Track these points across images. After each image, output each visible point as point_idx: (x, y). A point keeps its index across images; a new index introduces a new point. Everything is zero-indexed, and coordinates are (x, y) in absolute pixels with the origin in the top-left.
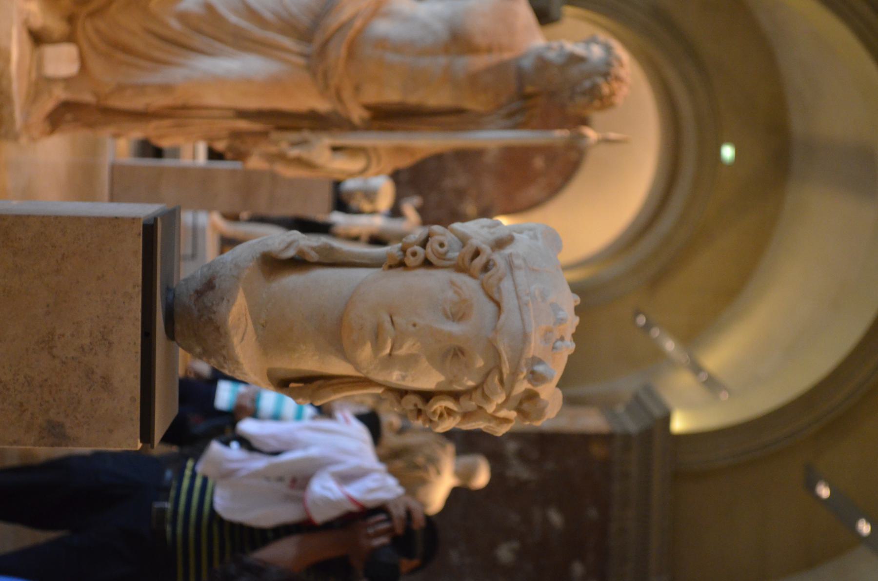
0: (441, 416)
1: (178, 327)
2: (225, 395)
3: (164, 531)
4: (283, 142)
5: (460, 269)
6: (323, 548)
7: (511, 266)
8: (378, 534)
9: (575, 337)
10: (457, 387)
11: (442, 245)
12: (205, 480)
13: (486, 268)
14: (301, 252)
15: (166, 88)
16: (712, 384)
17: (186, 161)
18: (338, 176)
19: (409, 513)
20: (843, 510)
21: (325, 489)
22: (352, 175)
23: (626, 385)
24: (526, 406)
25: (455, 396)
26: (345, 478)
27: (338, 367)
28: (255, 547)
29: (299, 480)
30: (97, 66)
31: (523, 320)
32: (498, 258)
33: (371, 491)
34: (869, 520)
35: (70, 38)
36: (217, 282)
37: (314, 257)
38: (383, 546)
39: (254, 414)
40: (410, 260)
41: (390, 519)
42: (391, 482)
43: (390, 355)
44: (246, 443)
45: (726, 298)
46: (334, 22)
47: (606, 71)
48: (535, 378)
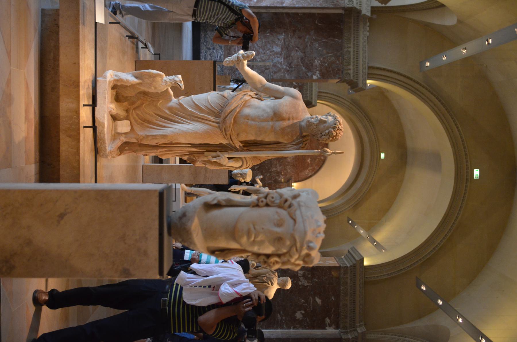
0: (274, 264)
1: (173, 231)
2: (188, 255)
3: (166, 309)
4: (210, 156)
5: (280, 206)
6: (226, 313)
7: (299, 206)
8: (247, 307)
9: (325, 232)
10: (280, 252)
11: (273, 198)
12: (182, 288)
13: (290, 206)
14: (219, 202)
15: (164, 136)
16: (378, 246)
17: (172, 164)
18: (231, 169)
19: (259, 297)
20: (432, 295)
21: (226, 289)
22: (236, 168)
23: (345, 248)
24: (306, 259)
25: (279, 256)
26: (233, 285)
27: (234, 245)
28: (201, 315)
29: (215, 287)
30: (137, 128)
31: (304, 226)
32: (294, 202)
33: (245, 289)
34: (441, 300)
35: (127, 118)
36: (187, 214)
37: (224, 203)
38: (249, 311)
39: (199, 262)
40: (261, 204)
41: (252, 300)
42: (252, 286)
43: (254, 241)
44: (194, 273)
45: (383, 212)
46: (228, 109)
47: (335, 126)
48: (310, 248)
